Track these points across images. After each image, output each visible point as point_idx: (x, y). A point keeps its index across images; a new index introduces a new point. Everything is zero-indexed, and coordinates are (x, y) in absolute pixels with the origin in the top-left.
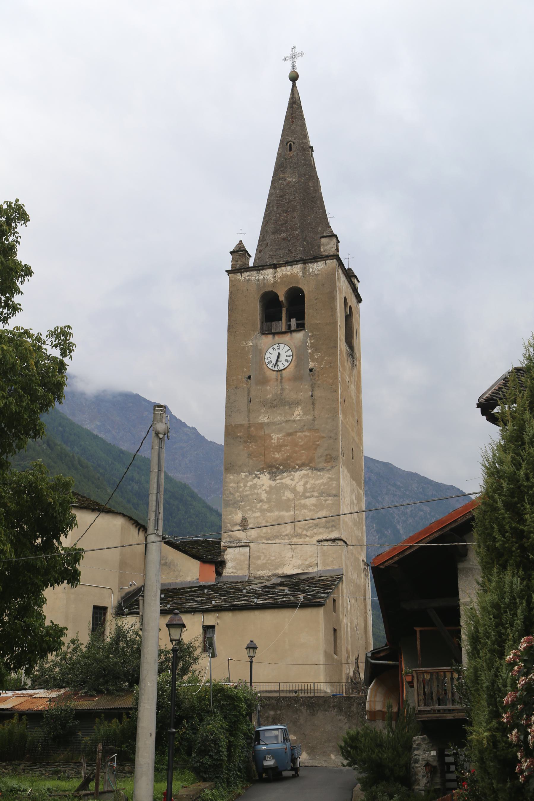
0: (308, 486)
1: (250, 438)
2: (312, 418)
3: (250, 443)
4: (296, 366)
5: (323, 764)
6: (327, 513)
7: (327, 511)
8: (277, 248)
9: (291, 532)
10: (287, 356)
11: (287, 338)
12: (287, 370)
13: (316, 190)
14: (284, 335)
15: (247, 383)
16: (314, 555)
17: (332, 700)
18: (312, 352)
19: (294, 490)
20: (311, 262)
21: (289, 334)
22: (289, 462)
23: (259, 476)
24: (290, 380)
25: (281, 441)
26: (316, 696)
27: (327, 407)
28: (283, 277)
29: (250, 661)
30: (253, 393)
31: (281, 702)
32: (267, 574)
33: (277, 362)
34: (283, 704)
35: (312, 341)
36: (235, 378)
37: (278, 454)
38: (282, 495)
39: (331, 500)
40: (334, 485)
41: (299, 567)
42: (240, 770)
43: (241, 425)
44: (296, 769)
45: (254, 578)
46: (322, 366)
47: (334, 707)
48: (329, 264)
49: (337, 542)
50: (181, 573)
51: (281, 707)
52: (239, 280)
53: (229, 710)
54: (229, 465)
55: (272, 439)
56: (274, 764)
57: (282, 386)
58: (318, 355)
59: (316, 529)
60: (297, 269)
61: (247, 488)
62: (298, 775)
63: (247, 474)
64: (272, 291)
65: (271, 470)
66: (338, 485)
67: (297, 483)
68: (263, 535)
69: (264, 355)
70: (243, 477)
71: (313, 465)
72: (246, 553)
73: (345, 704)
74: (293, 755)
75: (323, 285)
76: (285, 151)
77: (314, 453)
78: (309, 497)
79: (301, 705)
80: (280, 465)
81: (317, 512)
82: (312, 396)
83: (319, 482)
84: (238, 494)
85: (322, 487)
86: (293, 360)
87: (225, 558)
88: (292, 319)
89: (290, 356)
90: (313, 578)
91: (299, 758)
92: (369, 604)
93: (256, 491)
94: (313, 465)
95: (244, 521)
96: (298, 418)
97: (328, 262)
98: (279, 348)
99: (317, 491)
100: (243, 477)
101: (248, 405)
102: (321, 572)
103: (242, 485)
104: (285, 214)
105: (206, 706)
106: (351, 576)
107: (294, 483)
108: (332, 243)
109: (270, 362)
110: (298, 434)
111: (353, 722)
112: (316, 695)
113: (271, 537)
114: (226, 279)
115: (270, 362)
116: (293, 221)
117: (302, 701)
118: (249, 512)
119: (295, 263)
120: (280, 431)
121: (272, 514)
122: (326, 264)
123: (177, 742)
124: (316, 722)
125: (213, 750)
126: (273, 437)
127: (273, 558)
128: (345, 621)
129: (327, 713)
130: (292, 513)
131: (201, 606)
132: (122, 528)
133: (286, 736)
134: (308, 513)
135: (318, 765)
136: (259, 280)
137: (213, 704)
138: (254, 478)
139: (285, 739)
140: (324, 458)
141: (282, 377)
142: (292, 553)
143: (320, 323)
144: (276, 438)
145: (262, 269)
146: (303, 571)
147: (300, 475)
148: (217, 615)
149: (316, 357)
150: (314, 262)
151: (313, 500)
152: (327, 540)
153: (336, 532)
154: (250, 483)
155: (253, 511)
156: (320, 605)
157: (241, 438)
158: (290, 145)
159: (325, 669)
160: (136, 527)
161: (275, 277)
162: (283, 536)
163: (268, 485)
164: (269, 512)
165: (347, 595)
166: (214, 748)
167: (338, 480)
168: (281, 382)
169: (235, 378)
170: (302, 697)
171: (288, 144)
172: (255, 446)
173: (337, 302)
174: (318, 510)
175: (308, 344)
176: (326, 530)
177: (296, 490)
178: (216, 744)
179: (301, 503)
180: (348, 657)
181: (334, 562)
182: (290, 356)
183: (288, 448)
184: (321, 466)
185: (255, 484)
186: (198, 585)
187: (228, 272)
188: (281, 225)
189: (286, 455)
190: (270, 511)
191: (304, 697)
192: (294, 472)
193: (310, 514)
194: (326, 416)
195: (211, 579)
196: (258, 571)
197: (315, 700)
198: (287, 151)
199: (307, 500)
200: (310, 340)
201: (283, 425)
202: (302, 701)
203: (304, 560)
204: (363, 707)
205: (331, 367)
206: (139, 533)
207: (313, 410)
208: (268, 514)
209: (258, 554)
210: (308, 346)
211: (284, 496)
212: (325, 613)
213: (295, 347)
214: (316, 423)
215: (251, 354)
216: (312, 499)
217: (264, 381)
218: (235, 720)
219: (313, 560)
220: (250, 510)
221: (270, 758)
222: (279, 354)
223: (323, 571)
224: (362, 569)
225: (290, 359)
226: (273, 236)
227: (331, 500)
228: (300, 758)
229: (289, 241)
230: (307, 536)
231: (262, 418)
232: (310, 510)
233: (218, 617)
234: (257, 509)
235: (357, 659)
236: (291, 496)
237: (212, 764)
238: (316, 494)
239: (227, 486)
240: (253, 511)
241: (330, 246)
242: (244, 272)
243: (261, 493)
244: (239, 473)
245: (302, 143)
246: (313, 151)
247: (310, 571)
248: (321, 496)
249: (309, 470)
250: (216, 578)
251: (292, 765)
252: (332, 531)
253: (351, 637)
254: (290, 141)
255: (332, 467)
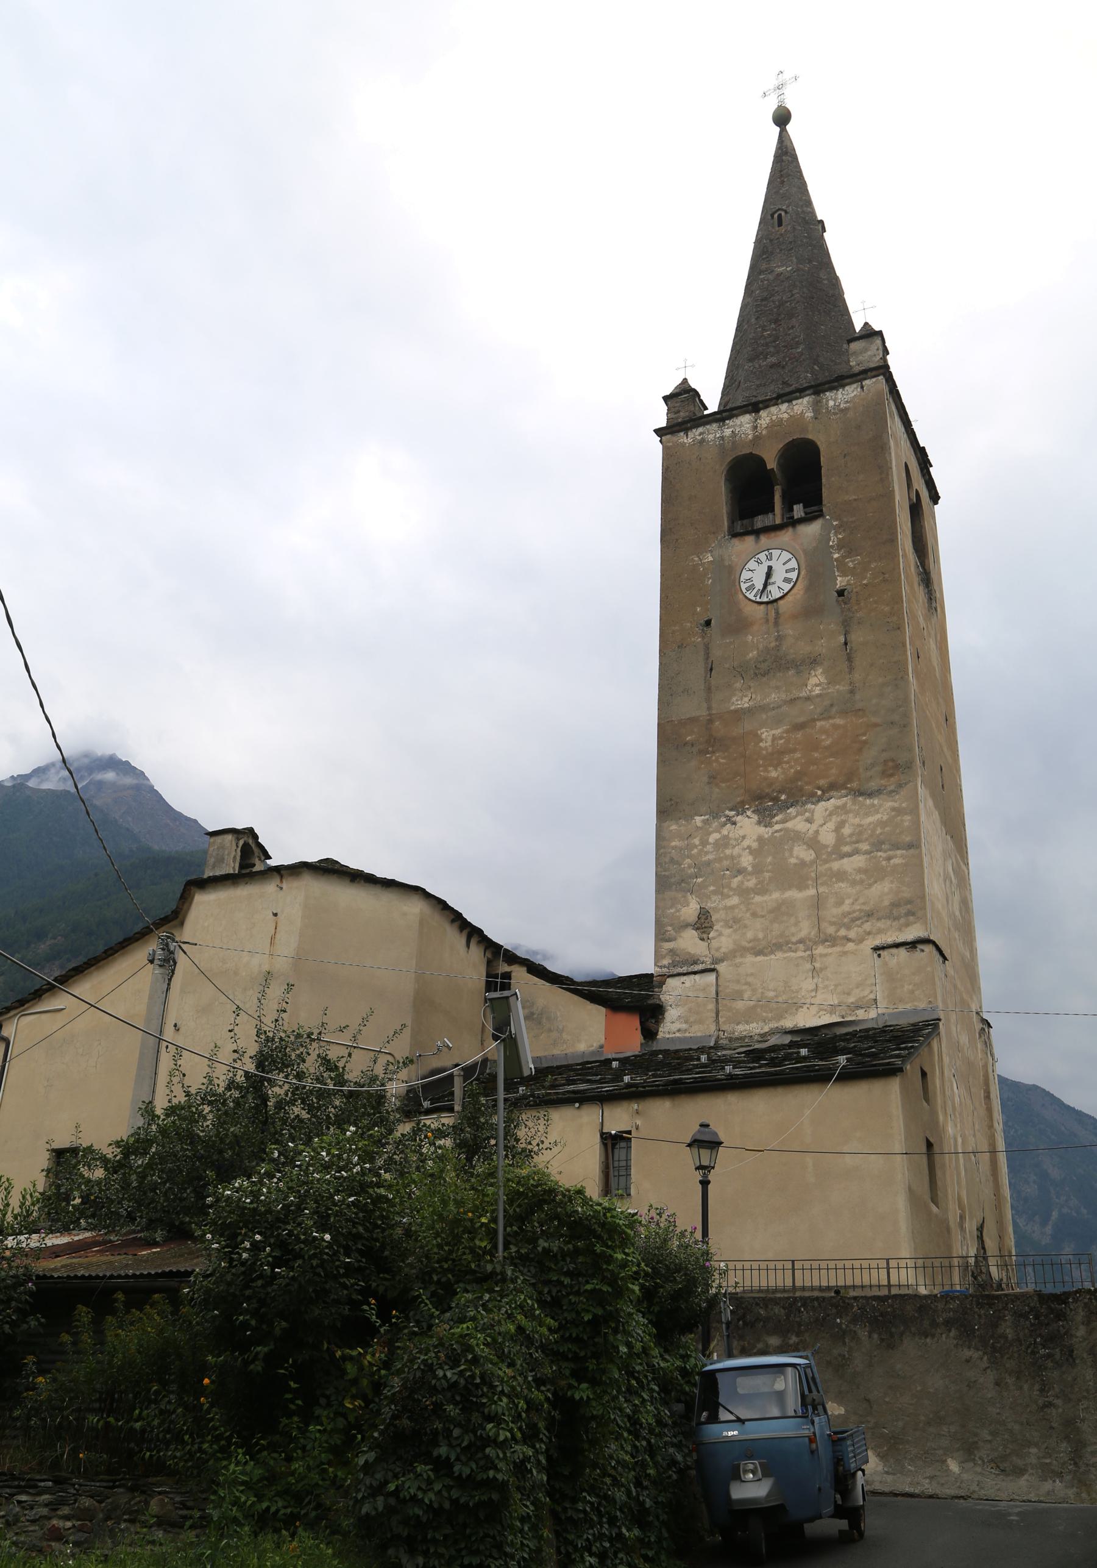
0: (847, 831)
1: (713, 743)
2: (847, 688)
3: (713, 752)
4: (808, 589)
5: (928, 1487)
6: (893, 886)
7: (892, 882)
8: (758, 383)
9: (810, 933)
10: (787, 571)
11: (786, 536)
12: (789, 598)
13: (834, 285)
14: (778, 533)
15: (704, 635)
16: (869, 982)
17: (940, 1306)
18: (842, 556)
19: (813, 843)
20: (831, 389)
21: (790, 529)
22: (800, 783)
23: (734, 819)
24: (794, 617)
25: (782, 741)
26: (895, 1296)
27: (881, 661)
28: (771, 426)
29: (701, 1182)
30: (716, 653)
31: (800, 1311)
32: (758, 1031)
33: (765, 585)
34: (805, 1315)
35: (840, 536)
36: (677, 628)
37: (776, 770)
38: (787, 854)
39: (902, 856)
40: (906, 824)
41: (832, 1009)
42: (639, 1518)
43: (693, 720)
44: (852, 1514)
45: (730, 1041)
46: (865, 582)
47: (948, 1324)
48: (868, 385)
49: (920, 946)
50: (565, 1036)
51: (800, 1324)
52: (683, 445)
53: (569, 1274)
54: (669, 803)
55: (761, 740)
56: (768, 1495)
57: (778, 632)
58: (854, 560)
59: (869, 923)
60: (802, 406)
61: (709, 848)
62: (861, 1534)
63: (707, 817)
64: (751, 453)
65: (760, 804)
66: (917, 824)
67: (821, 826)
68: (747, 945)
69: (737, 577)
70: (699, 824)
71: (855, 785)
72: (708, 986)
73: (980, 1316)
74: (838, 1461)
75: (858, 427)
76: (770, 228)
77: (858, 761)
78: (849, 855)
79: (855, 1320)
80: (781, 792)
81: (870, 885)
82: (846, 644)
83: (870, 819)
84: (688, 861)
85: (879, 831)
86: (801, 576)
87: (663, 999)
88: (795, 507)
89: (793, 570)
90: (867, 1030)
91: (860, 1473)
92: (996, 1109)
93: (728, 852)
94: (855, 785)
95: (704, 917)
96: (817, 690)
97: (867, 382)
98: (769, 558)
99: (867, 839)
100: (699, 824)
101: (706, 677)
102: (886, 1017)
103: (697, 841)
104: (773, 326)
105: (478, 1258)
106: (955, 1035)
107: (814, 827)
108: (874, 347)
109: (751, 588)
110: (819, 724)
111: (1007, 1365)
112: (894, 1291)
113: (764, 948)
114: (656, 447)
115: (751, 588)
116: (789, 335)
117: (856, 1308)
118: (714, 898)
119: (798, 394)
120: (778, 722)
121: (766, 898)
122: (862, 387)
123: (354, 1398)
124: (899, 1366)
125: (456, 1432)
126: (764, 736)
127: (771, 994)
128: (950, 1130)
129: (928, 1340)
130: (812, 892)
131: (598, 1088)
132: (422, 923)
133: (810, 1391)
134: (849, 890)
135: (911, 1490)
136: (722, 438)
137: (506, 1247)
138: (725, 824)
139: (810, 1405)
140: (879, 768)
141: (777, 613)
142: (815, 980)
143: (855, 500)
144: (770, 738)
145: (730, 418)
146: (843, 1018)
147: (826, 810)
148: (636, 1106)
149: (851, 565)
150: (836, 388)
151: (859, 861)
152: (897, 945)
153: (918, 926)
154: (714, 837)
155: (722, 894)
156: (891, 1071)
157: (692, 745)
158: (780, 216)
159: (913, 1233)
160: (461, 931)
161: (756, 427)
162: (793, 943)
163: (755, 837)
164: (758, 894)
165: (951, 1070)
166: (458, 1425)
167: (914, 811)
168: (776, 623)
169: (677, 628)
170: (855, 1298)
171: (776, 216)
172: (724, 758)
173: (890, 453)
174: (872, 880)
175: (831, 543)
176: (894, 924)
177: (819, 842)
178: (468, 1405)
179: (830, 869)
180: (962, 1217)
181: (917, 993)
182: (793, 570)
183: (798, 755)
184: (873, 785)
185: (726, 837)
186: (603, 1059)
187: (659, 432)
188: (767, 345)
189: (792, 771)
190: (761, 890)
191: (862, 1297)
192: (813, 803)
193: (854, 891)
194: (880, 680)
195: (632, 1043)
196: (738, 1024)
197: (892, 1306)
198: (773, 227)
199: (845, 860)
200: (836, 534)
201: (785, 708)
202: (856, 1308)
203: (844, 993)
204: (1032, 1325)
205: (885, 581)
206: (468, 946)
207: (850, 673)
208: (758, 899)
209: (737, 987)
210: (832, 547)
211: (791, 856)
212: (905, 1091)
213: (804, 551)
214: (857, 697)
215: (709, 578)
216: (856, 858)
217: (739, 626)
218: (595, 1316)
219: (866, 993)
220: (714, 892)
221: (754, 1472)
222: (770, 568)
223: (890, 1015)
224: (977, 1031)
225: (793, 575)
226: (750, 364)
227: (902, 856)
228: (863, 1471)
229: (783, 367)
230: (849, 940)
231: (737, 700)
232: (854, 883)
233: (637, 1112)
234: (731, 889)
235: (980, 1229)
236: (808, 855)
237: (447, 1505)
238: (865, 847)
239: (664, 847)
240: (722, 894)
241: (869, 353)
242: (691, 428)
243: (740, 856)
244: (689, 817)
245: (803, 212)
246: (824, 230)
247: (860, 1018)
248: (877, 851)
249: (846, 796)
250: (641, 1044)
251: (838, 1496)
252: (907, 925)
253: (966, 1171)
254: (779, 210)
255: (900, 786)
